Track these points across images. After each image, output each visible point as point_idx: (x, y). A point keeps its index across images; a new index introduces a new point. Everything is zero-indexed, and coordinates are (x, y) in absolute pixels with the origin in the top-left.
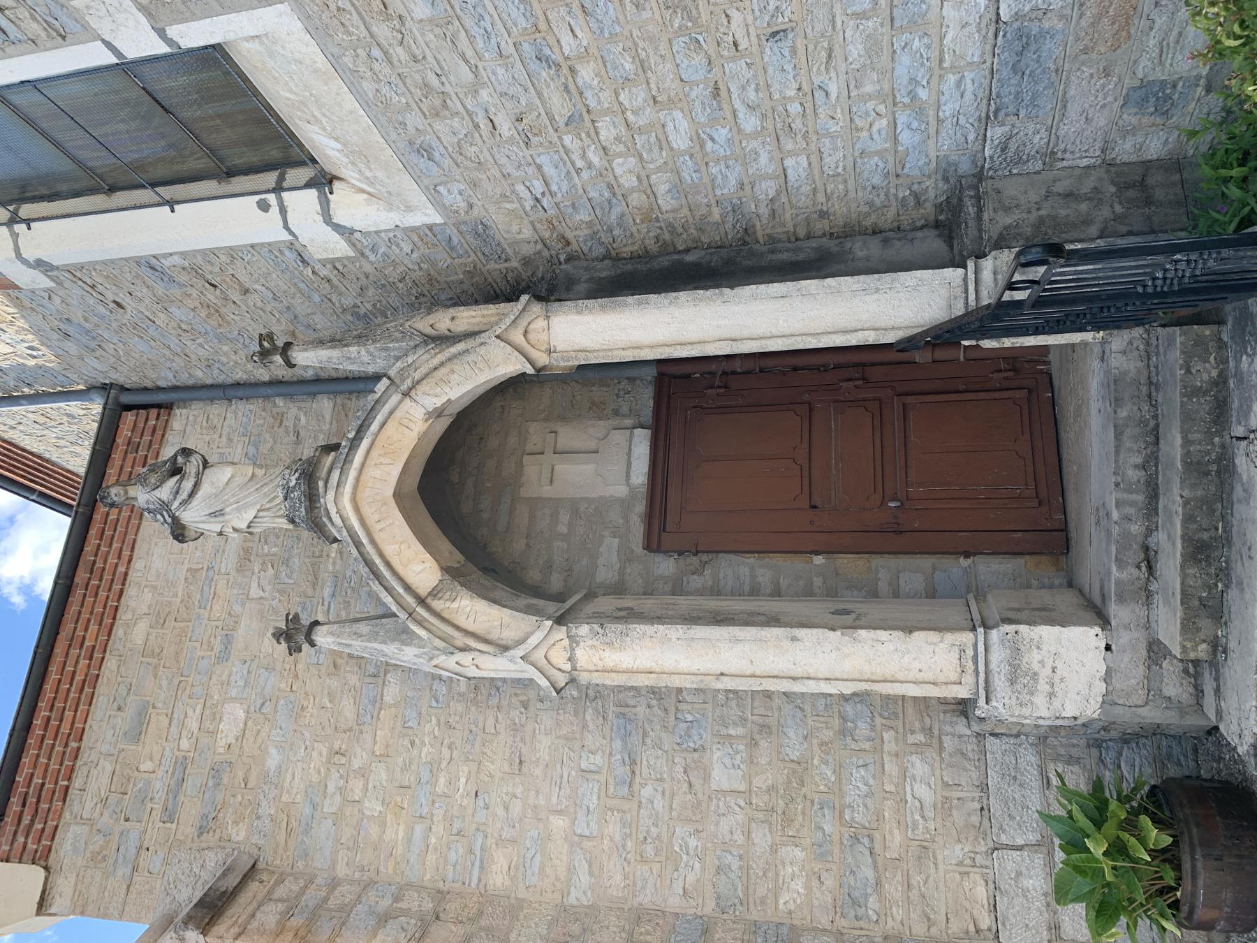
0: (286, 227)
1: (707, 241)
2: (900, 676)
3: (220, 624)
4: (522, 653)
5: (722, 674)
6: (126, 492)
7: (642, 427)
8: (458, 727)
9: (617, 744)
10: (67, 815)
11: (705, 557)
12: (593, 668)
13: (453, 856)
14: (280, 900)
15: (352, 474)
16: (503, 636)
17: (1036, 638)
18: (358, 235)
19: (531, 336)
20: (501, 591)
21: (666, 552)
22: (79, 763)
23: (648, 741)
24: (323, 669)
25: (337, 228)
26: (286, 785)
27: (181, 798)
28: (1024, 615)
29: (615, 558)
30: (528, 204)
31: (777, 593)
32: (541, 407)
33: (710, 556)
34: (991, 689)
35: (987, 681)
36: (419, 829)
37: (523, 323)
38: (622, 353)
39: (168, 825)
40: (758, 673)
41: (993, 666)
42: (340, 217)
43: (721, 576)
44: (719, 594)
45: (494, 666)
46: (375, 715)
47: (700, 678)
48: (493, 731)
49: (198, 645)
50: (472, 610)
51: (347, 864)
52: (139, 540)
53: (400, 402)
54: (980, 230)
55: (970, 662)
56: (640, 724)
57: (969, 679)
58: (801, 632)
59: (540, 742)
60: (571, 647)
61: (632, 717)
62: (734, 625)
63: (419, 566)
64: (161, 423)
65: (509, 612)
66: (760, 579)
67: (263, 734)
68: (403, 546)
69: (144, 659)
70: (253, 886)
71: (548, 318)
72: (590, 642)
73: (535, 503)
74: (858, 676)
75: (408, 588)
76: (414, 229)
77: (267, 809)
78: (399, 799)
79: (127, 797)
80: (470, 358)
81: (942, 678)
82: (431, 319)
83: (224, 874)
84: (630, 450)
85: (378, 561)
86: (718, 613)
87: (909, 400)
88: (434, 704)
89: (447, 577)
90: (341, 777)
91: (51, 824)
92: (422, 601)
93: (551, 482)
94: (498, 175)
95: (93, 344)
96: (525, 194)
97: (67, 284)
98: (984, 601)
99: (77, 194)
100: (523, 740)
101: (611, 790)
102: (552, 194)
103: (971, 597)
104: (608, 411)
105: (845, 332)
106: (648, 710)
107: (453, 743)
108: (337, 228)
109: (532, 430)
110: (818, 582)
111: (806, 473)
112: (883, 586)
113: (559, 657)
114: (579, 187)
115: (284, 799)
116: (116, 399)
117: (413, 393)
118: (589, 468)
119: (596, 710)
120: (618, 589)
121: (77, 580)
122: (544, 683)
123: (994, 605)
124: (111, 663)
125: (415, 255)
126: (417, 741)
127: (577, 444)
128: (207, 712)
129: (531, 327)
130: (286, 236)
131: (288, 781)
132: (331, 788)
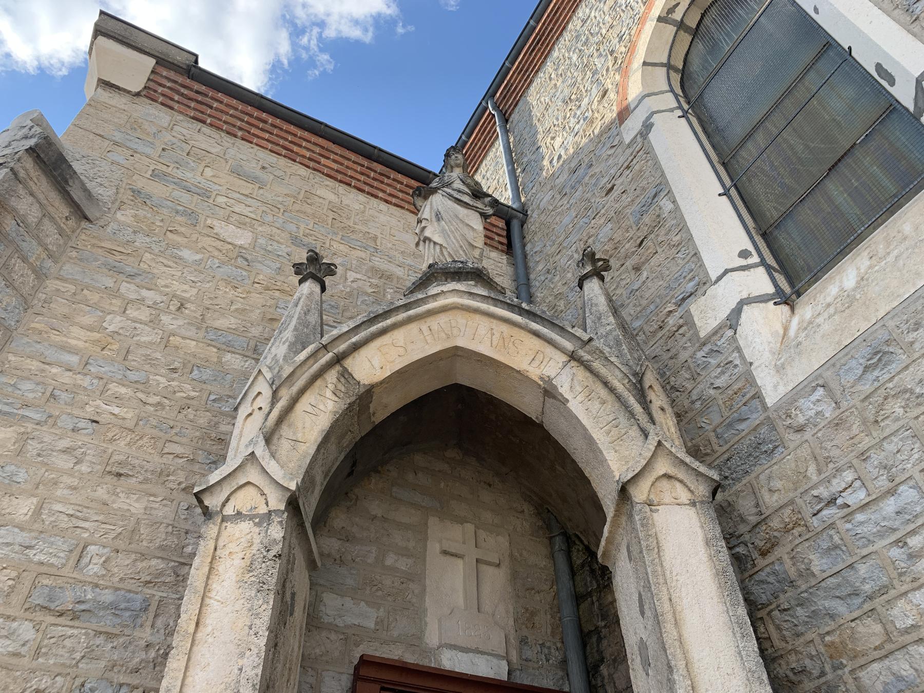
0: (726, 272)
3: (327, 245)
4: (258, 453)
6: (458, 166)
8: (180, 416)
9: (107, 596)
10: (181, 117)
12: (221, 543)
13: (26, 386)
14: (40, 222)
15: (484, 306)
16: (283, 441)
18: (730, 333)
19: (665, 483)
20: (336, 456)
22: (223, 134)
23: (100, 640)
24: (271, 310)
25: (737, 312)
26: (161, 259)
27: (172, 186)
29: (350, 620)
30: (823, 492)
32: (525, 553)
36: (74, 359)
38: (665, 598)
39: (150, 172)
42: (748, 312)
45: (246, 433)
46: (213, 343)
48: (166, 450)
49: (310, 227)
50: (318, 413)
51: (58, 290)
52: (403, 211)
53: (562, 350)
56: (127, 631)
59: (137, 500)
60: (255, 516)
61: (139, 621)
63: (374, 364)
64: (496, 244)
65: (312, 451)
67: (216, 253)
68: (402, 351)
69: (303, 192)
70: (65, 211)
71: (693, 504)
72: (257, 540)
73: (422, 532)
75: (356, 347)
76: (750, 380)
77: (141, 241)
78: (115, 347)
79: (185, 154)
80: (623, 420)
82: (657, 387)
83: (86, 190)
85: (389, 322)
88: (212, 397)
89: (362, 390)
90: (155, 303)
91: (176, 106)
92: (339, 359)
94: (862, 447)
95: (567, 190)
96: (837, 485)
97: (629, 151)
99: (713, 147)
100: (146, 481)
101: (46, 582)
102: (848, 518)
104: (525, 632)
106: (143, 643)
107: (163, 409)
108: (737, 312)
113: (245, 501)
114: (871, 549)
115: (147, 255)
116: (516, 217)
117: (573, 363)
119: (161, 574)
120: (313, 622)
121: (375, 164)
122: (214, 478)
124: (303, 171)
125: (712, 392)
126: (176, 375)
127: (486, 589)
128: (248, 220)
129: (678, 485)
130: (713, 276)
131: (165, 261)
132: (145, 293)
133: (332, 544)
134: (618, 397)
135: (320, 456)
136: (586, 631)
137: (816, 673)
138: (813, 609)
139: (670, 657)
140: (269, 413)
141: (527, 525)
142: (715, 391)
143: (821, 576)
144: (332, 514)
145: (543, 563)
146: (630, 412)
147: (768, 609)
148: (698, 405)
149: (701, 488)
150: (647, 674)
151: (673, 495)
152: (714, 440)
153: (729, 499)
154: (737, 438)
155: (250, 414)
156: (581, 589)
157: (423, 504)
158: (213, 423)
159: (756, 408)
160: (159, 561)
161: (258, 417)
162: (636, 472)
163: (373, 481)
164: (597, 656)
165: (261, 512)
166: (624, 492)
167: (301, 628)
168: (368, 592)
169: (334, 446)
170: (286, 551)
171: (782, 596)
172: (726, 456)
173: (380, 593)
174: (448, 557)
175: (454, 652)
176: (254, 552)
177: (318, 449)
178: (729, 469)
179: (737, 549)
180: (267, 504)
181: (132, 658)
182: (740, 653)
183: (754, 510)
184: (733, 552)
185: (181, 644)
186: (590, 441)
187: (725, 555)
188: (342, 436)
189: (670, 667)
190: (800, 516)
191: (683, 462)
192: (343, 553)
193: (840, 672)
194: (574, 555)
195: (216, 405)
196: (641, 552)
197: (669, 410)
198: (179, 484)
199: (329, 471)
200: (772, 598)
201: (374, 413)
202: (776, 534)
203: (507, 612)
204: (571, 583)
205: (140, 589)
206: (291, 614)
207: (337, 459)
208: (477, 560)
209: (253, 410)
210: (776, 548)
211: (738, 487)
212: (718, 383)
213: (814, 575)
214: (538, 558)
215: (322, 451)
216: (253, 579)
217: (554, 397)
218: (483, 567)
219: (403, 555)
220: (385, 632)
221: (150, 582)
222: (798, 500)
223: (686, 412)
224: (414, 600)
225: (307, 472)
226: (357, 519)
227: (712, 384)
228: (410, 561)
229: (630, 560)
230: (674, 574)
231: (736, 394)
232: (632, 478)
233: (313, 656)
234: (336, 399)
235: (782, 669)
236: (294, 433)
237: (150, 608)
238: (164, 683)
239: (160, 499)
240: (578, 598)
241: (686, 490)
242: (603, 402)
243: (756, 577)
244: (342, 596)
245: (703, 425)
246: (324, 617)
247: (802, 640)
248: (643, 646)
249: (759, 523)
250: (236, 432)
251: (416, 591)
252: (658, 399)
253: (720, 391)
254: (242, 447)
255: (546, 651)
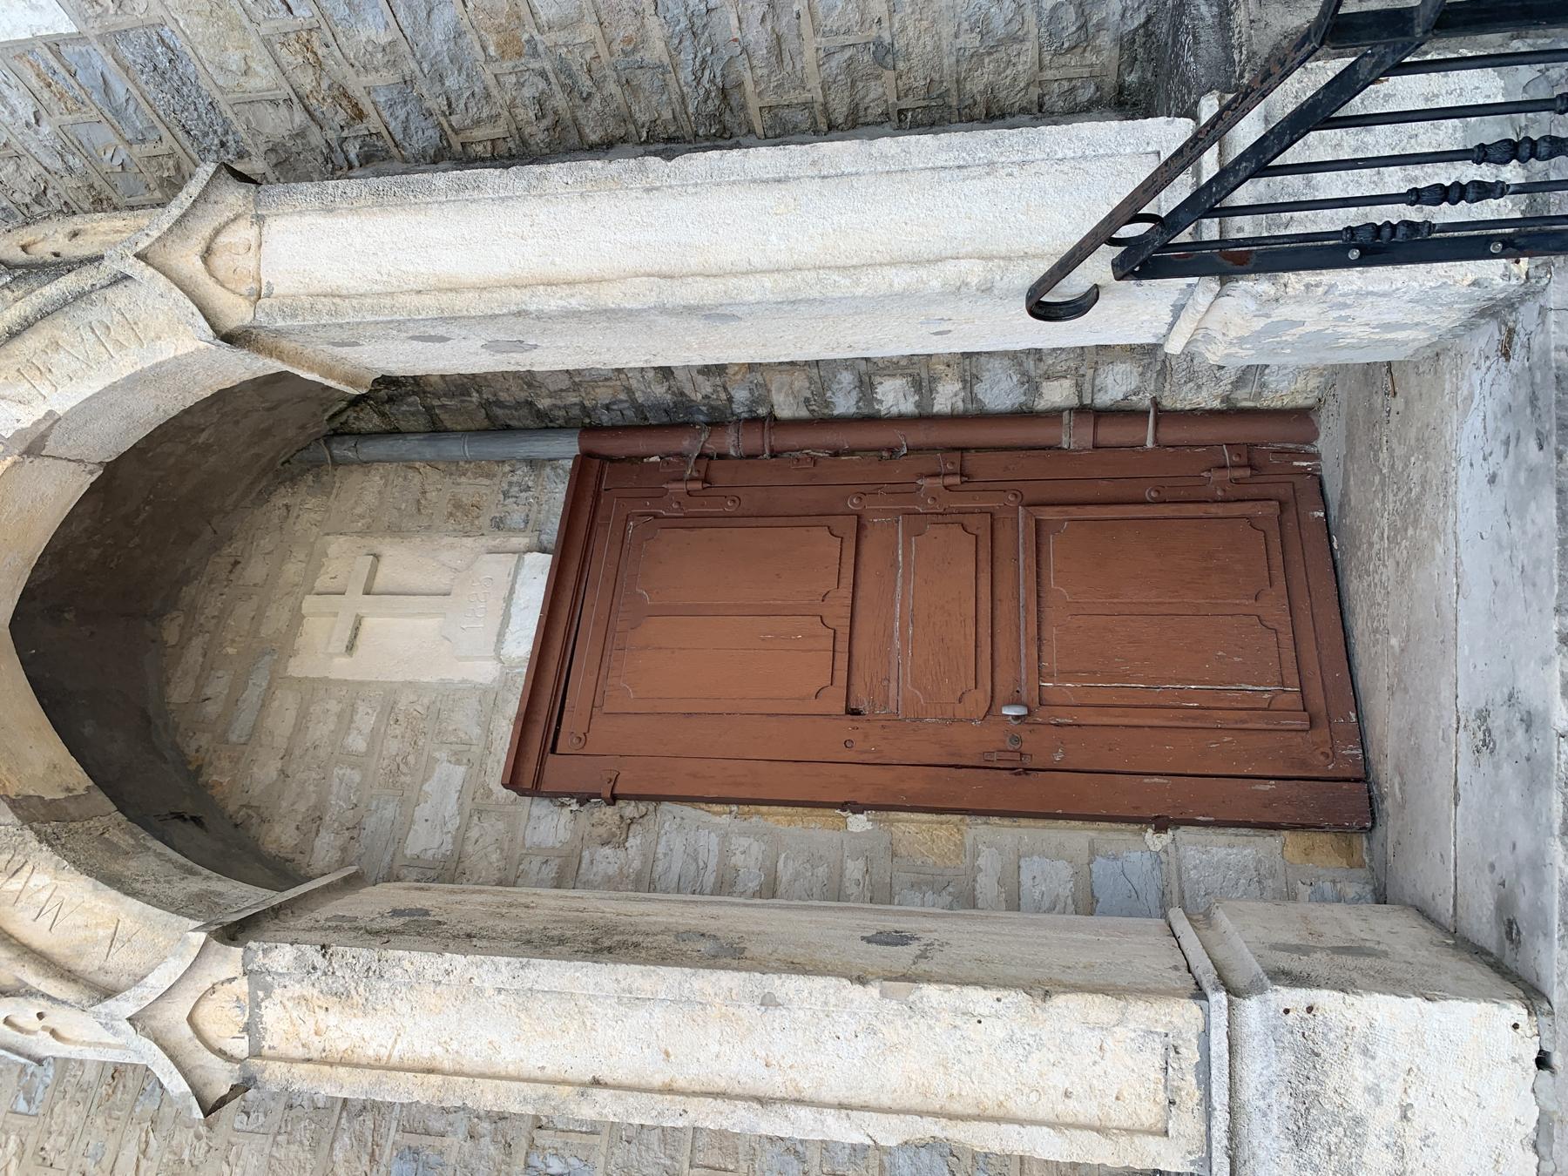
1: (643, 118)
2: (1018, 1106)
4: (131, 1009)
5: (596, 1083)
7: (544, 551)
8: (60, 1162)
11: (630, 809)
12: (300, 1052)
16: (111, 963)
17: (1360, 1025)
19: (218, 261)
20: (153, 859)
21: (553, 796)
28: (1317, 963)
29: (451, 807)
31: (769, 890)
32: (359, 510)
33: (642, 807)
34: (1244, 1154)
35: (1232, 1133)
37: (202, 230)
38: (416, 300)
40: (681, 1083)
41: (1248, 1093)
43: (661, 850)
44: (652, 887)
45: (89, 1036)
47: (543, 1089)
54: (1227, 47)
55: (1191, 1079)
57: (1187, 1124)
58: (788, 986)
61: (434, 1159)
62: (635, 960)
66: (738, 860)
71: (260, 220)
72: (296, 989)
74: (916, 1102)
80: (95, 314)
81: (1119, 1117)
82: (26, 235)
84: (512, 591)
86: (609, 930)
87: (1048, 514)
88: (22, 1106)
93: (350, 648)
98: (1210, 926)
103: (1176, 915)
104: (484, 521)
105: (915, 262)
109: (333, 550)
110: (854, 869)
111: (843, 646)
112: (987, 886)
113: (223, 1023)
118: (428, 625)
120: (448, 871)
122: (176, 1085)
123: (1243, 934)
125: (45, 129)
127: (414, 580)
129: (223, 239)
133: (325, 847)
134: (44, 315)
135: (149, 888)
136: (486, 423)
137: (542, 85)
138: (447, 60)
139: (505, 311)
140: (49, 998)
141: (311, 502)
142: (43, 123)
143: (394, 34)
144: (271, 847)
145: (375, 480)
146: (75, 299)
147: (449, 132)
148: (75, 162)
149: (231, 199)
150: (536, 347)
151: (242, 251)
152: (148, 149)
153: (263, 148)
154: (144, 106)
155: (53, 1033)
156: (422, 422)
157: (264, 684)
158: (79, 1096)
159: (81, 54)
160: (337, 1145)
161: (59, 1018)
162: (195, 310)
163: (215, 778)
164: (525, 411)
165: (246, 988)
166: (230, 338)
167: (452, 892)
168: (408, 779)
169: (133, 863)
170: (317, 936)
171: (428, 104)
172: (180, 134)
173: (411, 759)
174: (358, 642)
175: (509, 637)
176: (315, 992)
177: (134, 894)
178: (206, 135)
179: (352, 156)
180: (231, 980)
181: (490, 1158)
182: (502, 199)
183: (283, 109)
184: (357, 164)
185: (459, 1092)
186: (136, 381)
187: (351, 186)
188: (112, 847)
189: (519, 314)
190: (293, 36)
191: (180, 221)
192: (342, 825)
193: (541, 48)
194: (365, 426)
195: (39, 1096)
196: (341, 326)
197: (77, 222)
198: (198, 1137)
199: (182, 867)
200: (430, 120)
201: (68, 790)
202: (324, 85)
203: (452, 547)
204: (410, 437)
205: (382, 1169)
206: (427, 913)
207: (159, 855)
208: (367, 593)
209: (44, 1028)
210: (350, 92)
211: (239, 126)
212: (26, 111)
213: (393, 43)
214: (367, 488)
215: (138, 886)
216: (361, 989)
217: (43, 437)
218: (380, 582)
219: (351, 721)
220: (474, 748)
221: (372, 1154)
222: (265, 29)
223: (91, 186)
224: (426, 701)
225: (177, 912)
226: (284, 804)
227: (28, 124)
228: (362, 708)
229: (356, 344)
230: (378, 277)
231: (49, 85)
232: (207, 319)
233: (502, 864)
234: (27, 868)
235: (538, 134)
236: (97, 943)
237: (413, 1145)
238: (515, 1108)
239: (225, 1168)
240: (436, 429)
241: (233, 227)
242: (57, 346)
243: (399, 137)
244: (412, 822)
245: (117, 161)
246: (443, 850)
247: (494, 92)
248: (493, 346)
249: (306, 109)
250: (90, 1055)
251: (413, 698)
252: (51, 239)
253: (43, 112)
254: (120, 1040)
255: (515, 489)
